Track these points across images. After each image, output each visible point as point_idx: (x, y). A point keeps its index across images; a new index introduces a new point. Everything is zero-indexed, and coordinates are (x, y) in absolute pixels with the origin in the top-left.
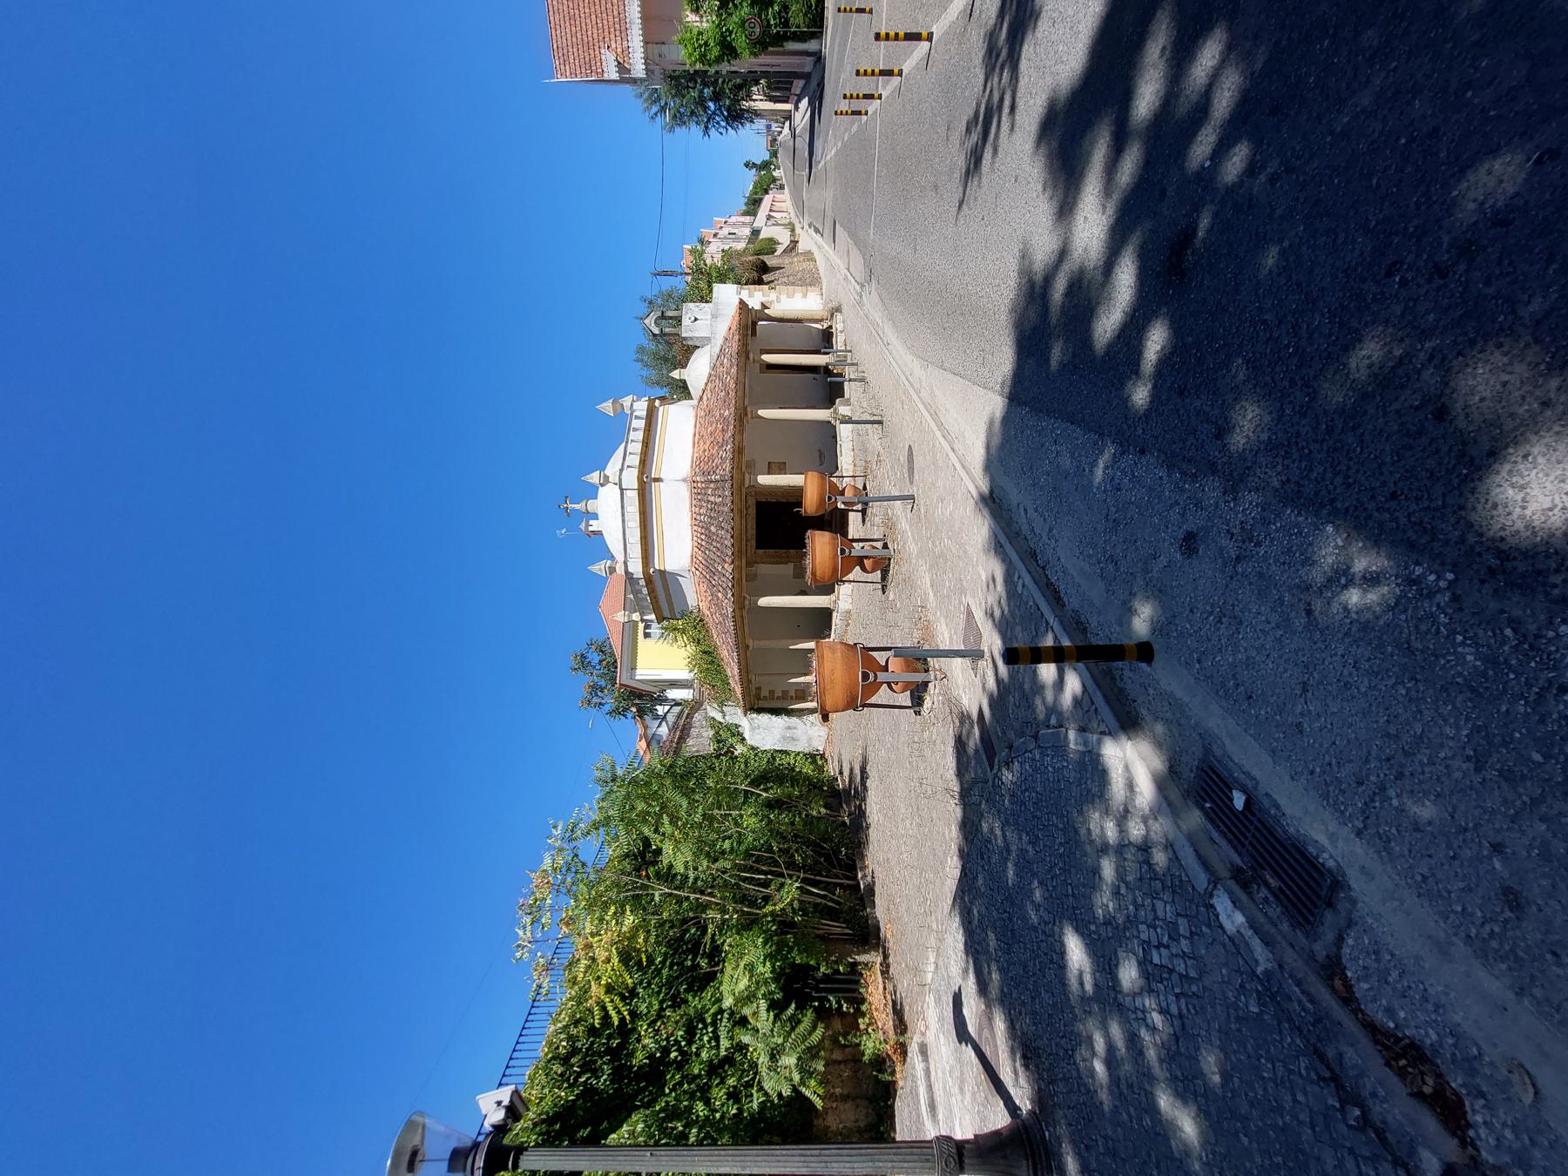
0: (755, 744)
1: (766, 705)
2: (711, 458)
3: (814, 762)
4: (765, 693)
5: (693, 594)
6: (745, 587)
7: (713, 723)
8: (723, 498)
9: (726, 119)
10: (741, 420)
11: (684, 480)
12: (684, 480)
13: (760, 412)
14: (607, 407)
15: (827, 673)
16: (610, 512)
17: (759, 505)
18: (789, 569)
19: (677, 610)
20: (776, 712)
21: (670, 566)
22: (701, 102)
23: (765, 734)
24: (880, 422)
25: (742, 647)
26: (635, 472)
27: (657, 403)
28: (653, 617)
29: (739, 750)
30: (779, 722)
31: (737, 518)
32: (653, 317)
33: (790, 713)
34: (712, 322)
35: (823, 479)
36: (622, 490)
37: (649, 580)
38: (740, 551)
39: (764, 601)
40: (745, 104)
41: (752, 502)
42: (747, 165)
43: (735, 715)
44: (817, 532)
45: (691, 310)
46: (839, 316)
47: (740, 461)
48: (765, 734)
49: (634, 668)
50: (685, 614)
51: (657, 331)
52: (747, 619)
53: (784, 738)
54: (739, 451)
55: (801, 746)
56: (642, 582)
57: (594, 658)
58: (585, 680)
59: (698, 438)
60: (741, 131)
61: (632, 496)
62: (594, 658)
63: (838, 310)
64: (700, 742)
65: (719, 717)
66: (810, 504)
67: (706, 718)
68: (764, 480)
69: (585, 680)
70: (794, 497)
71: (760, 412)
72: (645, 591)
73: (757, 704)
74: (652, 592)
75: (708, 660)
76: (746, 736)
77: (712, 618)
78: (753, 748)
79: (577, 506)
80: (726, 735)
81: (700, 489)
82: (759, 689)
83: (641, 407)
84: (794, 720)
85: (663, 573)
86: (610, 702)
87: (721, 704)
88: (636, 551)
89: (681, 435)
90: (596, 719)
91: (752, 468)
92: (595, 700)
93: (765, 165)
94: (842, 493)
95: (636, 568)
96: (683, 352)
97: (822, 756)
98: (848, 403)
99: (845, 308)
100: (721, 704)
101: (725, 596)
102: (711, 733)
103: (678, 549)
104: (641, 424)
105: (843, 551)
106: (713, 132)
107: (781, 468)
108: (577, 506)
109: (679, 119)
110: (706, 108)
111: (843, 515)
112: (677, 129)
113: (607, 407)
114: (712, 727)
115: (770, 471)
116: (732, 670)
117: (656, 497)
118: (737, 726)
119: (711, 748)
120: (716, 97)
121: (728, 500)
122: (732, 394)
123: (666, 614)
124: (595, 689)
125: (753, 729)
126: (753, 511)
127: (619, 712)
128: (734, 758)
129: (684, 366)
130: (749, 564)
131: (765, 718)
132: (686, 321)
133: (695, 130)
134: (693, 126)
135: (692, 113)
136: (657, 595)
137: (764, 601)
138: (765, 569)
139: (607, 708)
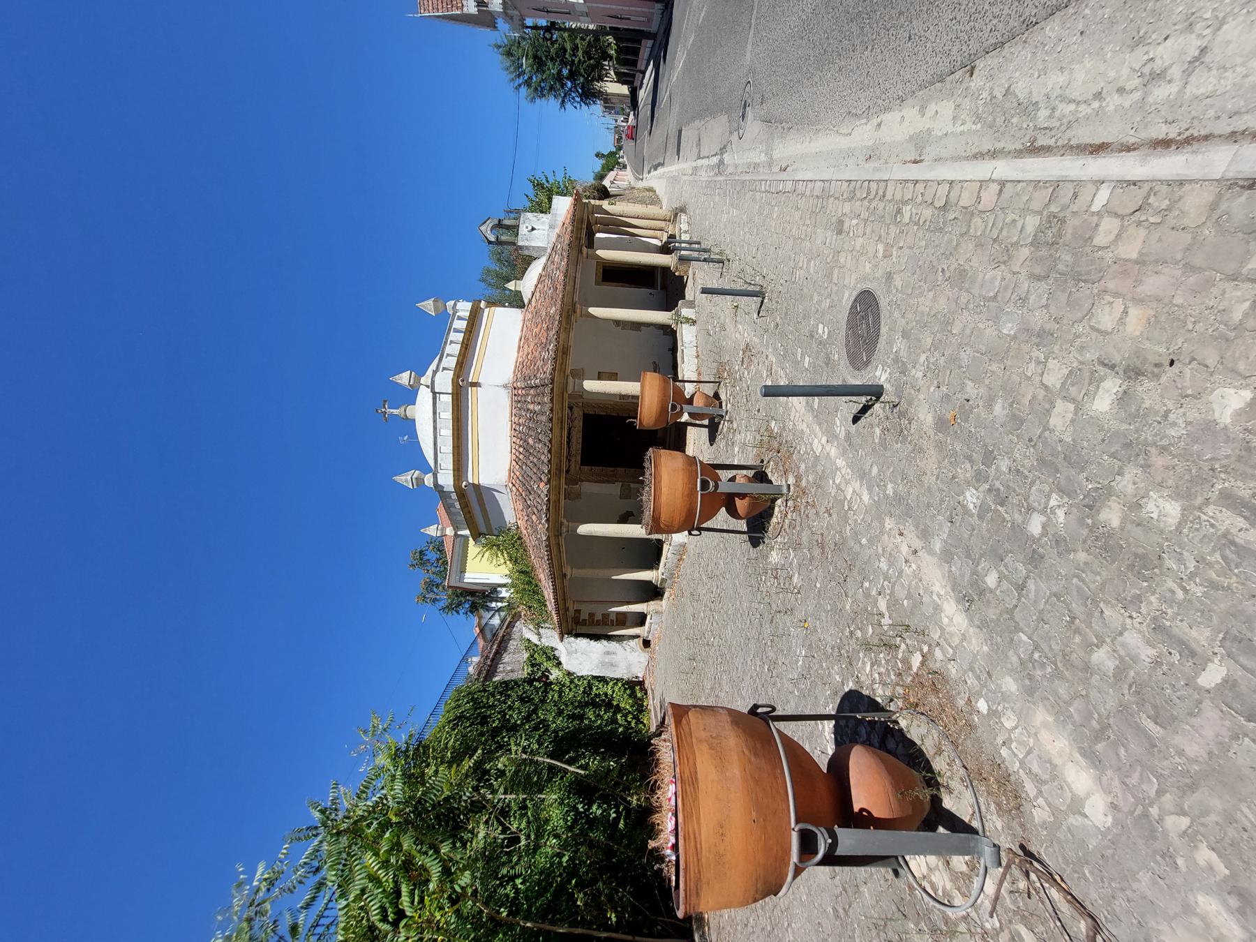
0: (572, 669)
1: (585, 630)
2: (533, 361)
3: (633, 695)
4: (584, 616)
5: (510, 511)
6: (562, 511)
7: (529, 645)
8: (541, 406)
9: (580, 96)
10: (568, 317)
11: (505, 386)
12: (505, 386)
13: (592, 310)
14: (428, 306)
15: (706, 833)
16: (427, 416)
17: (587, 418)
18: (614, 489)
19: (488, 525)
20: (595, 637)
21: (484, 481)
22: (559, 78)
23: (582, 658)
24: (760, 294)
25: (558, 577)
26: (450, 375)
27: (483, 304)
28: (467, 532)
29: (555, 674)
30: (597, 648)
31: (556, 430)
32: (490, 224)
33: (609, 638)
34: (544, 231)
35: (666, 382)
36: (434, 393)
37: (461, 494)
38: (559, 469)
39: (585, 529)
40: (598, 85)
41: (578, 413)
42: (597, 155)
43: (550, 638)
44: (664, 453)
45: (529, 220)
46: (683, 217)
47: (563, 364)
48: (582, 658)
49: (463, 571)
50: (503, 530)
51: (492, 239)
52: (561, 542)
53: (603, 664)
54: (562, 352)
55: (621, 672)
56: (454, 496)
57: (432, 555)
58: (422, 576)
59: (524, 339)
60: (593, 107)
61: (446, 400)
62: (432, 555)
63: (682, 210)
64: (514, 665)
65: (534, 639)
66: (648, 414)
67: (522, 639)
68: (591, 385)
69: (422, 576)
70: (630, 405)
71: (592, 310)
72: (457, 505)
73: (578, 625)
74: (465, 506)
75: (525, 576)
76: (562, 660)
77: (530, 541)
78: (569, 674)
79: (395, 411)
80: (542, 657)
81: (521, 393)
82: (578, 611)
83: (464, 308)
84: (613, 645)
85: (477, 488)
86: (444, 598)
87: (538, 626)
88: (447, 462)
89: (505, 342)
90: (430, 614)
91: (580, 375)
92: (431, 595)
93: (612, 154)
94: (690, 401)
95: (446, 479)
96: (519, 262)
97: (641, 683)
98: (691, 305)
99: (690, 209)
100: (538, 626)
101: (540, 519)
102: (526, 655)
103: (494, 462)
104: (461, 325)
105: (705, 485)
106: (568, 105)
107: (613, 377)
108: (395, 411)
109: (539, 92)
110: (563, 85)
111: (681, 430)
112: (538, 100)
113: (428, 306)
114: (527, 649)
115: (600, 377)
116: (548, 594)
117: (478, 406)
118: (553, 649)
119: (524, 673)
120: (573, 76)
121: (547, 408)
122: (560, 287)
123: (483, 529)
124: (431, 586)
125: (569, 653)
126: (579, 424)
127: (452, 608)
128: (548, 684)
129: (521, 278)
130: (571, 482)
131: (583, 643)
132: (523, 230)
133: (552, 103)
134: (552, 99)
135: (552, 88)
136: (473, 507)
137: (585, 529)
138: (588, 487)
139: (442, 604)
